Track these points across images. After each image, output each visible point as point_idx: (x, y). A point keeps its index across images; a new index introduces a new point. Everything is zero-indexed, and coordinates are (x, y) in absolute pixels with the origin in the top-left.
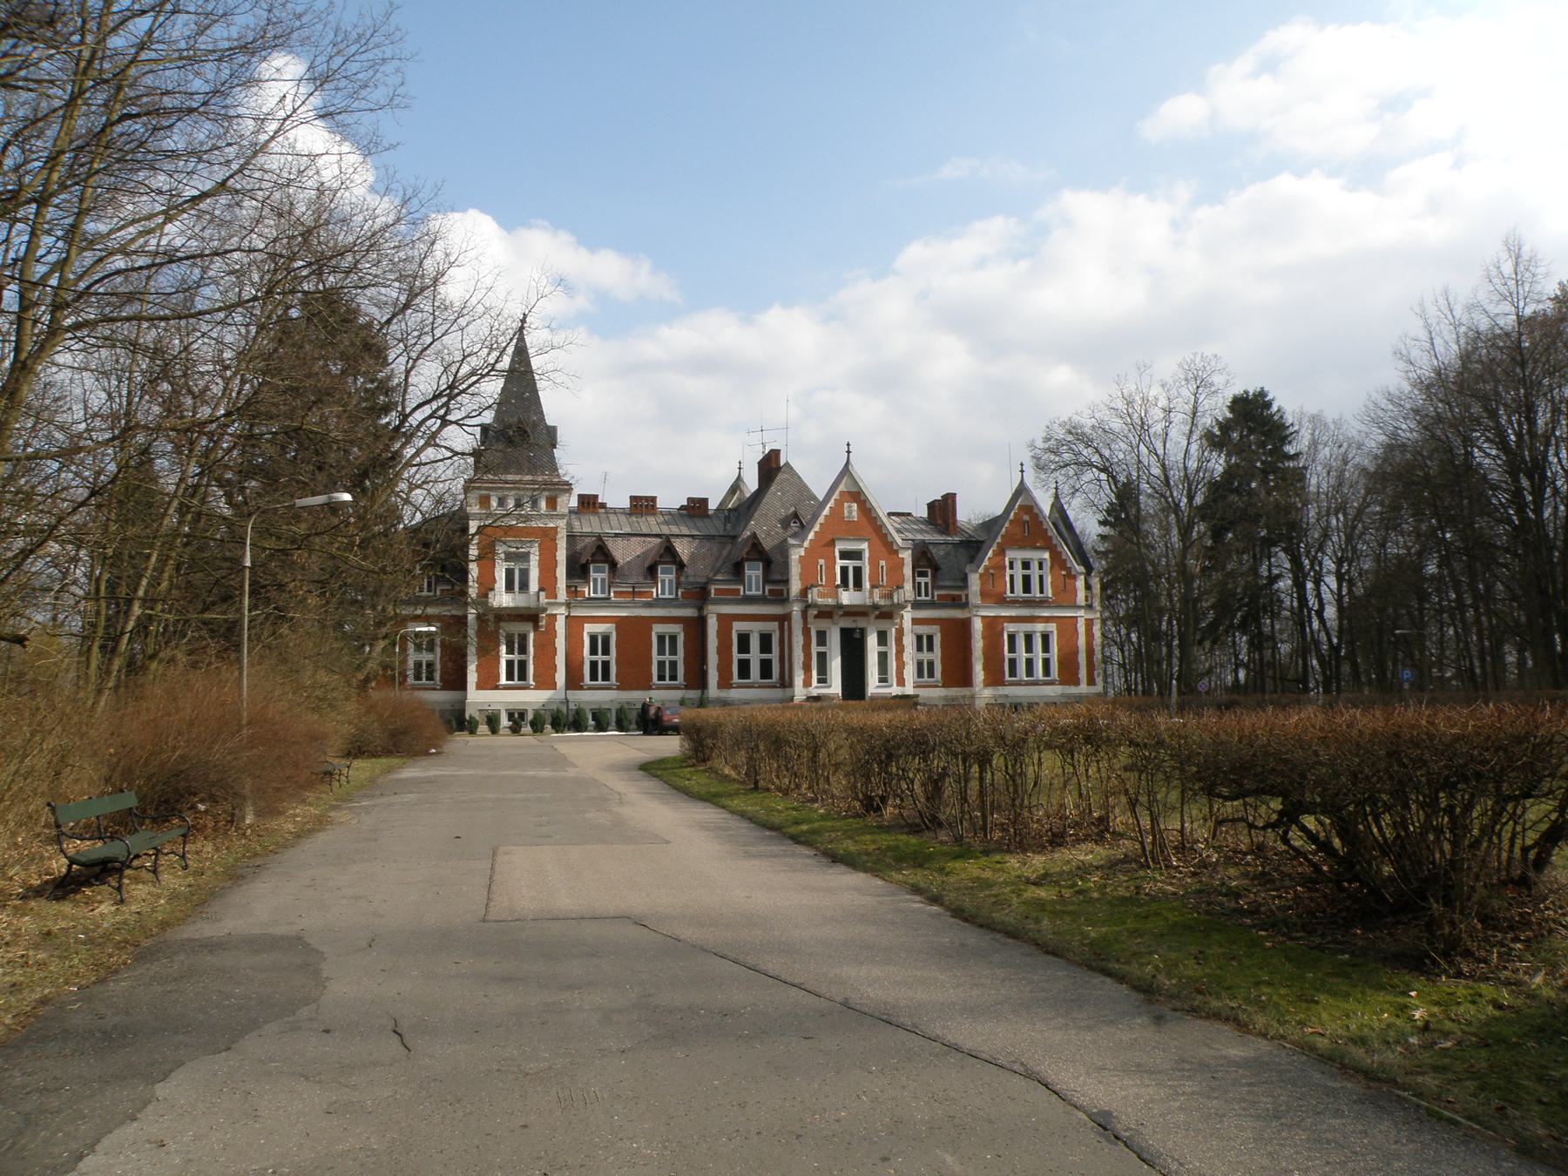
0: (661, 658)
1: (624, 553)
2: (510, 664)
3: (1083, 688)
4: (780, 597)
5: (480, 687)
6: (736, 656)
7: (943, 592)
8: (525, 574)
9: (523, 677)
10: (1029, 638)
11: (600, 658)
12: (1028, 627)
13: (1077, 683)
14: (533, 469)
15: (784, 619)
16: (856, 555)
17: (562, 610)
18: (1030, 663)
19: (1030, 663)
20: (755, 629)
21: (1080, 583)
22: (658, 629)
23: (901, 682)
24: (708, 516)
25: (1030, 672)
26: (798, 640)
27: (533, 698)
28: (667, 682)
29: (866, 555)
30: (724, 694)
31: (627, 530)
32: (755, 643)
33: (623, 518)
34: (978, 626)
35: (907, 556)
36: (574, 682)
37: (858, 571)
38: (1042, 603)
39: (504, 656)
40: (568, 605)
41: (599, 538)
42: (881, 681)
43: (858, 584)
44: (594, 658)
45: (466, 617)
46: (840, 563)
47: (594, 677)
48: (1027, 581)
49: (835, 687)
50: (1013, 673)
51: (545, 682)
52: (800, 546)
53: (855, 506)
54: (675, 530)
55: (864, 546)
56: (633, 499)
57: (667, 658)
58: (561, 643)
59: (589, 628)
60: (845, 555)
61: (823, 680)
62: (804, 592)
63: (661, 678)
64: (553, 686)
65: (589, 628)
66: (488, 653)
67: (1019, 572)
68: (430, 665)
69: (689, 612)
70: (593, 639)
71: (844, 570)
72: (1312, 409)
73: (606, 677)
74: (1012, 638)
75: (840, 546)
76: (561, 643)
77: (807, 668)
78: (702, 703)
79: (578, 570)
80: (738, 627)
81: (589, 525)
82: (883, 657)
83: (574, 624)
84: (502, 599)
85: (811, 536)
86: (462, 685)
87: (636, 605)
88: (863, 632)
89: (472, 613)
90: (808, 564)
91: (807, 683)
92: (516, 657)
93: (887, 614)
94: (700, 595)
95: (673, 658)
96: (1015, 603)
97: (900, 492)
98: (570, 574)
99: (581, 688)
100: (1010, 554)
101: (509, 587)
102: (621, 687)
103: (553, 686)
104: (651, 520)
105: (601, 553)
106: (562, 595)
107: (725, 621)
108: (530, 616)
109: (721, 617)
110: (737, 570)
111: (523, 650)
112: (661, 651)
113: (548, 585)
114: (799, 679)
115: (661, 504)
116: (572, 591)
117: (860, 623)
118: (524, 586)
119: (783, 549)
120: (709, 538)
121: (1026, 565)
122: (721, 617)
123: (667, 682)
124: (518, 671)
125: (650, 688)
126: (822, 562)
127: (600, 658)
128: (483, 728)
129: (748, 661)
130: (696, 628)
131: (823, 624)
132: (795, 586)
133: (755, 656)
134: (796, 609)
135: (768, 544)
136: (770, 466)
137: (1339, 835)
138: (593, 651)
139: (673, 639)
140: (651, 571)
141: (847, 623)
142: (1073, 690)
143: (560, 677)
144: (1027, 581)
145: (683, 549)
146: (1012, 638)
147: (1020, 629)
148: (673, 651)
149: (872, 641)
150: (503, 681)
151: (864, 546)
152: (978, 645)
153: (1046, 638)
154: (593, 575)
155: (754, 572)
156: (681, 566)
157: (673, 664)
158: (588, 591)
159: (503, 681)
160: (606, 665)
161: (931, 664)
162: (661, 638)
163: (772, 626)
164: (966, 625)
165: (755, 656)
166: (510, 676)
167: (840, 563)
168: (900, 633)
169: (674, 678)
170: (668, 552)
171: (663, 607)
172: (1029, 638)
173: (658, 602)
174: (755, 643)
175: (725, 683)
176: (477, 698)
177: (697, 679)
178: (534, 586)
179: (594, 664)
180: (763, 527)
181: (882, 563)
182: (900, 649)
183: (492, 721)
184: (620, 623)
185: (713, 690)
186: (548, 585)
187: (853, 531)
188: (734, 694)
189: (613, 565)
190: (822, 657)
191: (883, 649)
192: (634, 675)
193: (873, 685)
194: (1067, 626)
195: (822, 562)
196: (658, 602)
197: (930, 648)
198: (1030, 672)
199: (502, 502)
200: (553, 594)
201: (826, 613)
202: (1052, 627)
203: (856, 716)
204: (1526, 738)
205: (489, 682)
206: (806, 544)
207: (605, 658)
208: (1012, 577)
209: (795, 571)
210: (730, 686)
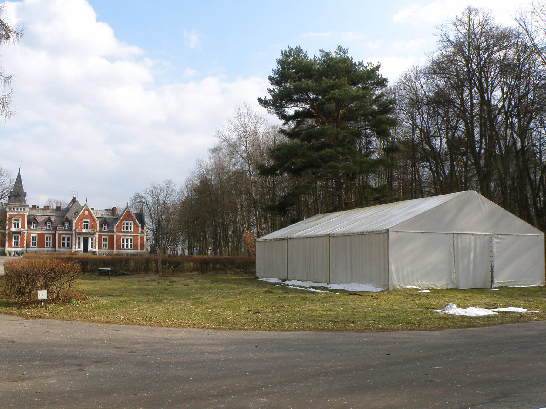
1: (40, 219)
2: (15, 242)
3: (139, 251)
4: (71, 230)
6: (62, 242)
8: (18, 224)
9: (17, 245)
10: (127, 240)
11: (34, 241)
13: (138, 249)
14: (20, 202)
15: (72, 234)
16: (87, 222)
17: (26, 232)
18: (127, 245)
19: (127, 245)
20: (66, 237)
21: (140, 228)
22: (46, 235)
23: (95, 248)
25: (127, 247)
26: (74, 239)
27: (19, 249)
30: (59, 249)
31: (41, 214)
32: (66, 239)
33: (42, 211)
34: (115, 237)
35: (98, 222)
36: (28, 246)
37: (87, 225)
38: (131, 232)
41: (35, 216)
43: (87, 228)
46: (83, 223)
47: (33, 245)
48: (127, 228)
50: (123, 247)
51: (22, 246)
54: (52, 214)
55: (89, 220)
57: (48, 242)
58: (25, 238)
59: (32, 235)
62: (75, 229)
64: (24, 247)
65: (32, 235)
66: (10, 240)
67: (126, 225)
68: (35, 237)
69: (53, 232)
70: (33, 237)
71: (84, 225)
72: (149, 187)
74: (123, 240)
75: (83, 220)
76: (25, 238)
77: (75, 245)
78: (55, 251)
79: (30, 223)
80: (63, 236)
81: (33, 213)
82: (92, 243)
83: (28, 234)
84: (13, 229)
86: (5, 246)
88: (88, 238)
90: (77, 224)
91: (75, 248)
92: (16, 241)
93: (93, 234)
94: (55, 229)
96: (124, 232)
97: (100, 205)
98: (28, 224)
100: (124, 222)
102: (39, 247)
103: (24, 247)
104: (48, 211)
105: (35, 220)
106: (26, 228)
107: (60, 235)
108: (19, 233)
110: (63, 224)
111: (18, 239)
113: (23, 226)
114: (74, 247)
116: (28, 227)
117: (87, 236)
118: (18, 227)
119: (72, 220)
120: (59, 216)
121: (127, 224)
124: (16, 244)
127: (34, 241)
128: (8, 255)
130: (54, 235)
131: (79, 236)
132: (74, 228)
133: (66, 242)
134: (74, 233)
135: (69, 219)
136: (74, 201)
137: (485, 159)
138: (33, 240)
139: (50, 238)
140: (46, 223)
141: (84, 236)
142: (136, 251)
143: (25, 244)
145: (53, 219)
146: (123, 240)
148: (50, 240)
149: (90, 240)
150: (13, 246)
151: (89, 220)
152: (115, 240)
153: (131, 240)
155: (66, 224)
156: (52, 223)
157: (50, 243)
158: (32, 227)
159: (13, 246)
161: (106, 244)
162: (47, 238)
163: (70, 236)
164: (114, 236)
165: (66, 242)
166: (15, 245)
167: (83, 223)
168: (96, 238)
170: (49, 219)
172: (127, 240)
173: (47, 230)
174: (66, 239)
175: (59, 247)
176: (8, 249)
177: (54, 246)
178: (20, 226)
179: (33, 243)
180: (69, 215)
182: (96, 242)
183: (10, 254)
184: (39, 234)
185: (57, 249)
186: (23, 226)
187: (86, 217)
188: (61, 249)
189: (37, 222)
190: (79, 243)
193: (89, 248)
194: (136, 238)
196: (47, 230)
198: (127, 247)
201: (80, 234)
203: (86, 255)
205: (10, 246)
209: (74, 225)
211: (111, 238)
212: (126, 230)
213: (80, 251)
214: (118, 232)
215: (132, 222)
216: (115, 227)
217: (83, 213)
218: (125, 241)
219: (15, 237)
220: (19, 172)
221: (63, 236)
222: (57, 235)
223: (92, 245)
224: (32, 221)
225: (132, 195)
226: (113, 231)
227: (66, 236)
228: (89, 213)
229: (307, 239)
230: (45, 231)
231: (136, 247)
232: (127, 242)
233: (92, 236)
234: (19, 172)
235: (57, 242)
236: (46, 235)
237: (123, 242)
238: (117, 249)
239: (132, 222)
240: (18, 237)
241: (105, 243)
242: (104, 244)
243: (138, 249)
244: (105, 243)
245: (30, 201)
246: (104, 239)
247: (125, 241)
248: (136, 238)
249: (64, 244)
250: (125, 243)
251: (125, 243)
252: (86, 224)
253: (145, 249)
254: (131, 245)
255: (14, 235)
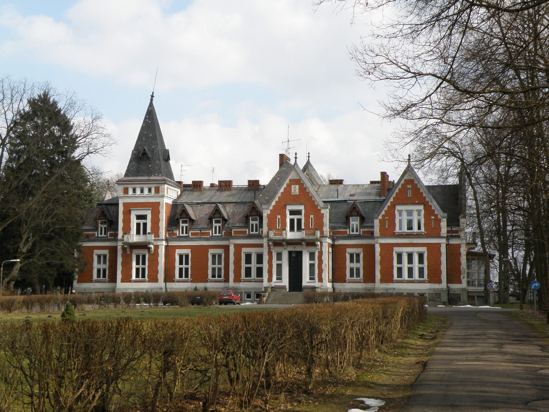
0: (214, 266)
2: (137, 270)
5: (123, 281)
6: (244, 265)
7: (366, 230)
9: (143, 276)
10: (410, 256)
12: (410, 249)
16: (298, 212)
17: (164, 243)
22: (211, 251)
23: (321, 280)
24: (261, 189)
28: (217, 278)
29: (303, 212)
30: (237, 285)
32: (254, 259)
34: (378, 249)
35: (326, 213)
36: (169, 278)
37: (299, 221)
38: (418, 236)
39: (134, 265)
40: (167, 240)
42: (311, 279)
44: (181, 266)
45: (117, 247)
48: (410, 223)
49: (285, 282)
51: (154, 279)
52: (268, 209)
53: (297, 187)
56: (250, 182)
60: (292, 213)
61: (279, 278)
63: (213, 276)
65: (178, 251)
68: (105, 256)
70: (181, 257)
71: (292, 221)
73: (358, 275)
74: (400, 256)
75: (289, 208)
79: (173, 223)
80: (245, 250)
82: (312, 266)
83: (169, 250)
84: (134, 238)
85: (273, 203)
87: (201, 239)
88: (299, 254)
89: (120, 244)
91: (270, 280)
92: (141, 266)
95: (220, 266)
96: (401, 236)
99: (174, 281)
100: (398, 208)
101: (138, 232)
107: (238, 247)
108: (144, 246)
109: (236, 246)
112: (214, 263)
115: (235, 184)
117: (298, 248)
121: (410, 213)
122: (236, 246)
123: (217, 278)
125: (207, 281)
126: (279, 217)
129: (250, 268)
133: (254, 265)
142: (436, 286)
143: (161, 276)
144: (410, 223)
147: (405, 250)
149: (306, 261)
150: (134, 277)
151: (302, 208)
152: (378, 258)
153: (421, 256)
154: (181, 225)
156: (225, 220)
159: (134, 277)
160: (187, 269)
161: (358, 270)
162: (214, 256)
163: (221, 251)
164: (373, 247)
165: (254, 265)
167: (289, 217)
168: (321, 253)
169: (220, 276)
170: (217, 211)
171: (214, 240)
172: (410, 256)
174: (254, 259)
175: (237, 279)
179: (181, 270)
181: (312, 216)
187: (296, 200)
188: (242, 285)
190: (279, 267)
191: (312, 262)
192: (200, 275)
193: (306, 280)
194: (434, 250)
195: (279, 217)
196: (212, 238)
197: (358, 261)
199: (134, 191)
200: (157, 235)
201: (277, 243)
202: (424, 249)
204: (413, 311)
205: (127, 278)
206: (271, 208)
207: (186, 266)
208: (400, 221)
210: (240, 281)
211: (370, 250)
212: (405, 229)
213: (284, 287)
214: (383, 234)
215: (421, 207)
216: (377, 222)
217: (288, 189)
218: (405, 258)
219: (138, 257)
220: (151, 105)
221: (245, 250)
222: (232, 249)
223: (312, 273)
224: (178, 215)
225: (37, 93)
226: (371, 235)
227: (254, 251)
228: (303, 189)
229: (206, 205)
230: (207, 239)
231: (434, 277)
232: (410, 261)
233: (312, 249)
234: (151, 105)
235: (232, 267)
236: (211, 251)
237: (400, 261)
238: (382, 281)
239: (421, 207)
240: (144, 257)
241: (355, 265)
242: (352, 270)
243: (440, 282)
244: (355, 265)
245: (183, 169)
246: (352, 255)
247: (405, 258)
248: (434, 250)
249: (248, 272)
250: (405, 265)
251: (405, 265)
252: (296, 217)
253: (464, 281)
254: (421, 270)
255: (135, 253)
